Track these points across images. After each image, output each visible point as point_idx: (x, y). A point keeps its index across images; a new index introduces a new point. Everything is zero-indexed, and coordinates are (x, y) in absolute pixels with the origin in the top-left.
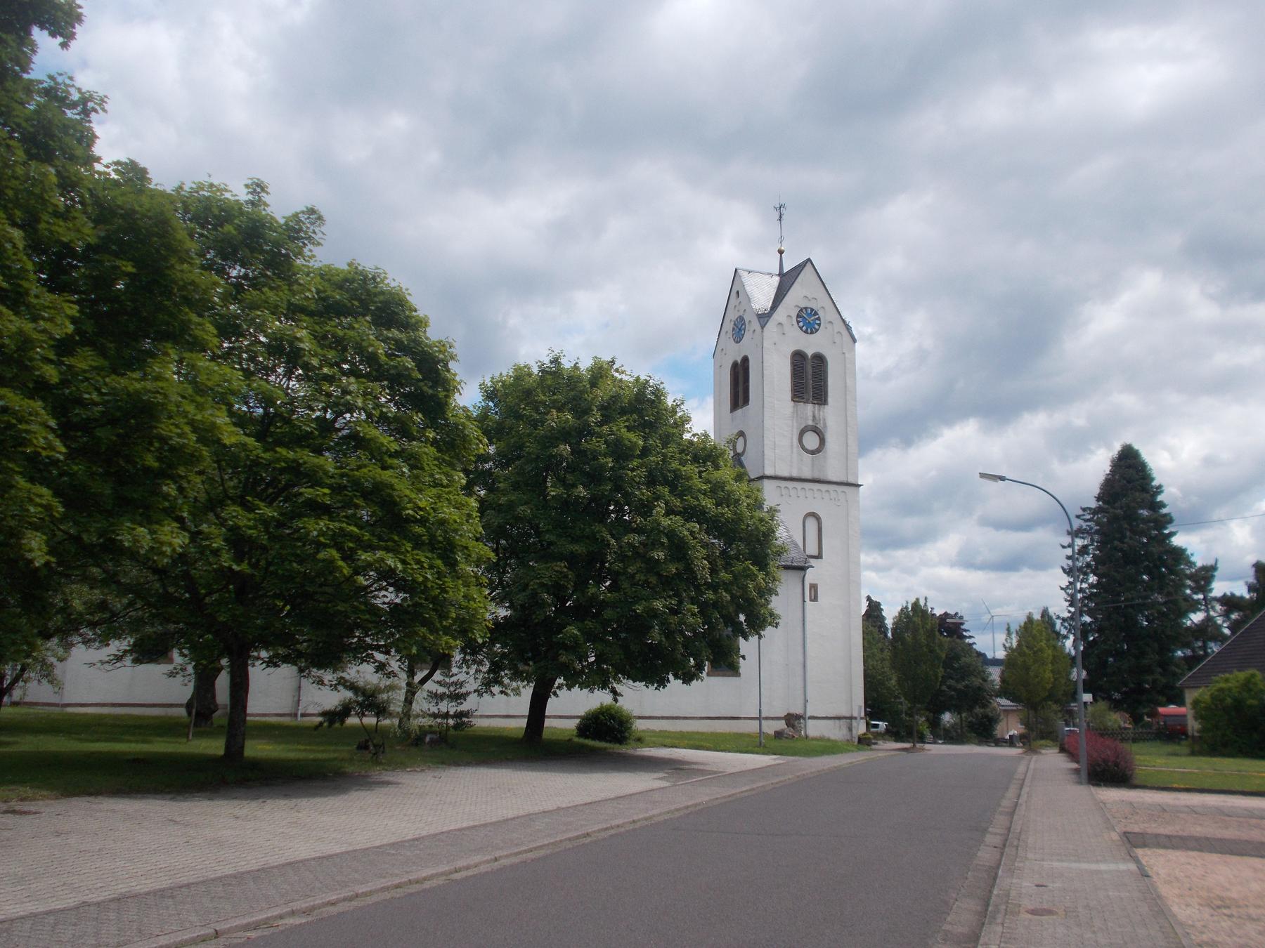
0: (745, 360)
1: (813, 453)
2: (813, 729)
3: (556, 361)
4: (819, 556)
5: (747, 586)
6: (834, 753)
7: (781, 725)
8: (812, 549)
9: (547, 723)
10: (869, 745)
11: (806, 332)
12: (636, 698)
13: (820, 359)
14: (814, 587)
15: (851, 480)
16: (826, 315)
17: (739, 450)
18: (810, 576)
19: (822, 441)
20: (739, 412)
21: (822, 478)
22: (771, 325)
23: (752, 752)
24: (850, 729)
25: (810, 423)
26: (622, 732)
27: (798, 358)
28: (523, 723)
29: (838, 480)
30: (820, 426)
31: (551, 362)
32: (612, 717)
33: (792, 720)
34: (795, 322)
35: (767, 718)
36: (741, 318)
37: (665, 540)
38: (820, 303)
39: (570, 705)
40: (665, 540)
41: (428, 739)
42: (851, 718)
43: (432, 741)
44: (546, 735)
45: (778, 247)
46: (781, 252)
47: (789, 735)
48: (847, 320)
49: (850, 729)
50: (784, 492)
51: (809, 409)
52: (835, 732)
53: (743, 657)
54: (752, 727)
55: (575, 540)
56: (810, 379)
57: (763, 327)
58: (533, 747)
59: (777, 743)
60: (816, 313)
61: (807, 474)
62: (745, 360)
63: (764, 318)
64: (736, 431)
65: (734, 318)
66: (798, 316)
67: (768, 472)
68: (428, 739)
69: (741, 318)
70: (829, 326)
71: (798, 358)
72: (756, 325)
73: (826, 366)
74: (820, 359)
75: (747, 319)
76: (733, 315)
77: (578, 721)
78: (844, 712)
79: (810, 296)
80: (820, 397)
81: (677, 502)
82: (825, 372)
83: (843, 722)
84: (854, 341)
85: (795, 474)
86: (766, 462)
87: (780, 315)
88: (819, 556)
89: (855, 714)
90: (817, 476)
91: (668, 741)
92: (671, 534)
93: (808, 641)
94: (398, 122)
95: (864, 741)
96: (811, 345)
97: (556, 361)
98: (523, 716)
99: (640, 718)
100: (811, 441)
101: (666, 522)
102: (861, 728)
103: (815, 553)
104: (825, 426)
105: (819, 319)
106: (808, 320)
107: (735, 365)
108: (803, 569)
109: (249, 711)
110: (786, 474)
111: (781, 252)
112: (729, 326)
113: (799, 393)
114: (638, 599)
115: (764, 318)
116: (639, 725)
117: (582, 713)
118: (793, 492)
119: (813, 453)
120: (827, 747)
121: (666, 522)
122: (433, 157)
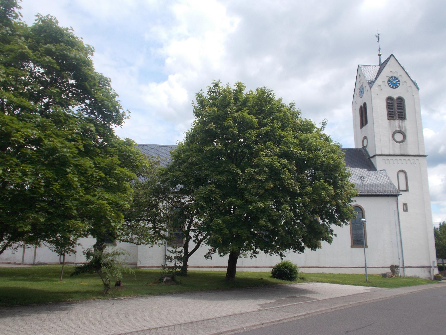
0: (365, 104)
1: (400, 142)
2: (409, 273)
3: (216, 85)
4: (407, 190)
5: (321, 194)
6: (416, 285)
7: (389, 271)
8: (403, 187)
9: (237, 270)
10: (440, 280)
11: (393, 88)
12: (291, 257)
13: (401, 100)
14: (405, 205)
15: (421, 154)
16: (403, 78)
17: (365, 145)
18: (402, 199)
19: (405, 137)
20: (364, 128)
21: (406, 154)
22: (375, 86)
23: (361, 285)
24: (430, 272)
25: (398, 129)
26: (291, 275)
27: (390, 100)
28: (226, 270)
29: (414, 154)
30: (403, 130)
31: (215, 86)
32: (286, 267)
33: (393, 268)
34: (386, 84)
35: (368, 267)
36: (362, 86)
37: (266, 169)
38: (399, 74)
39: (257, 263)
40: (266, 169)
41: (165, 280)
42: (430, 267)
43: (167, 281)
44: (237, 275)
45: (378, 53)
46: (380, 55)
47: (392, 276)
48: (414, 80)
49: (430, 272)
50: (386, 161)
51: (396, 123)
52: (423, 274)
53: (336, 235)
54: (362, 272)
55: (220, 173)
56: (396, 109)
57: (371, 88)
58: (230, 284)
59: (383, 280)
60: (397, 79)
61: (398, 152)
62: (365, 104)
63: (371, 83)
64: (363, 137)
65: (359, 87)
66: (388, 81)
67: (378, 153)
68: (165, 280)
69: (362, 86)
70: (404, 84)
71: (390, 100)
72: (368, 87)
73: (404, 102)
74: (401, 100)
75: (364, 86)
76: (358, 86)
77: (271, 269)
78: (426, 264)
79: (394, 71)
80: (402, 116)
81: (277, 149)
82: (404, 105)
83: (425, 269)
84: (418, 89)
85: (392, 153)
86: (376, 148)
87: (379, 81)
88: (407, 190)
89: (432, 265)
90: (403, 153)
91: (320, 279)
92: (271, 167)
93: (402, 230)
94: (268, 59)
95: (437, 278)
96: (395, 94)
97: (216, 85)
98: (226, 267)
99: (300, 267)
100: (399, 137)
101: (266, 159)
102: (436, 272)
103: (405, 189)
104: (406, 130)
105: (399, 81)
106: (394, 82)
107: (361, 108)
108: (396, 196)
109: (238, 265)
110: (387, 153)
111: (380, 55)
112: (357, 91)
113: (391, 116)
114: (251, 203)
115: (371, 83)
116: (300, 271)
117: (274, 265)
118: (391, 161)
119: (400, 142)
120: (413, 281)
121: (266, 159)
122: (280, 69)
